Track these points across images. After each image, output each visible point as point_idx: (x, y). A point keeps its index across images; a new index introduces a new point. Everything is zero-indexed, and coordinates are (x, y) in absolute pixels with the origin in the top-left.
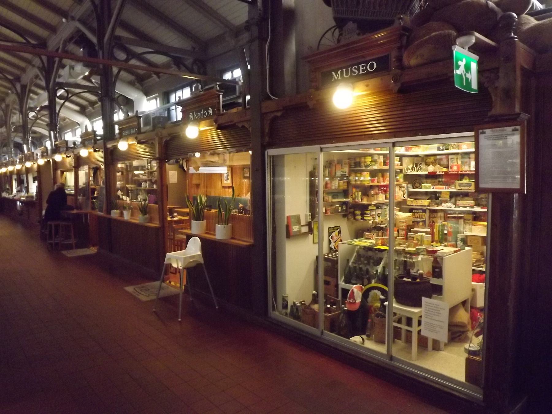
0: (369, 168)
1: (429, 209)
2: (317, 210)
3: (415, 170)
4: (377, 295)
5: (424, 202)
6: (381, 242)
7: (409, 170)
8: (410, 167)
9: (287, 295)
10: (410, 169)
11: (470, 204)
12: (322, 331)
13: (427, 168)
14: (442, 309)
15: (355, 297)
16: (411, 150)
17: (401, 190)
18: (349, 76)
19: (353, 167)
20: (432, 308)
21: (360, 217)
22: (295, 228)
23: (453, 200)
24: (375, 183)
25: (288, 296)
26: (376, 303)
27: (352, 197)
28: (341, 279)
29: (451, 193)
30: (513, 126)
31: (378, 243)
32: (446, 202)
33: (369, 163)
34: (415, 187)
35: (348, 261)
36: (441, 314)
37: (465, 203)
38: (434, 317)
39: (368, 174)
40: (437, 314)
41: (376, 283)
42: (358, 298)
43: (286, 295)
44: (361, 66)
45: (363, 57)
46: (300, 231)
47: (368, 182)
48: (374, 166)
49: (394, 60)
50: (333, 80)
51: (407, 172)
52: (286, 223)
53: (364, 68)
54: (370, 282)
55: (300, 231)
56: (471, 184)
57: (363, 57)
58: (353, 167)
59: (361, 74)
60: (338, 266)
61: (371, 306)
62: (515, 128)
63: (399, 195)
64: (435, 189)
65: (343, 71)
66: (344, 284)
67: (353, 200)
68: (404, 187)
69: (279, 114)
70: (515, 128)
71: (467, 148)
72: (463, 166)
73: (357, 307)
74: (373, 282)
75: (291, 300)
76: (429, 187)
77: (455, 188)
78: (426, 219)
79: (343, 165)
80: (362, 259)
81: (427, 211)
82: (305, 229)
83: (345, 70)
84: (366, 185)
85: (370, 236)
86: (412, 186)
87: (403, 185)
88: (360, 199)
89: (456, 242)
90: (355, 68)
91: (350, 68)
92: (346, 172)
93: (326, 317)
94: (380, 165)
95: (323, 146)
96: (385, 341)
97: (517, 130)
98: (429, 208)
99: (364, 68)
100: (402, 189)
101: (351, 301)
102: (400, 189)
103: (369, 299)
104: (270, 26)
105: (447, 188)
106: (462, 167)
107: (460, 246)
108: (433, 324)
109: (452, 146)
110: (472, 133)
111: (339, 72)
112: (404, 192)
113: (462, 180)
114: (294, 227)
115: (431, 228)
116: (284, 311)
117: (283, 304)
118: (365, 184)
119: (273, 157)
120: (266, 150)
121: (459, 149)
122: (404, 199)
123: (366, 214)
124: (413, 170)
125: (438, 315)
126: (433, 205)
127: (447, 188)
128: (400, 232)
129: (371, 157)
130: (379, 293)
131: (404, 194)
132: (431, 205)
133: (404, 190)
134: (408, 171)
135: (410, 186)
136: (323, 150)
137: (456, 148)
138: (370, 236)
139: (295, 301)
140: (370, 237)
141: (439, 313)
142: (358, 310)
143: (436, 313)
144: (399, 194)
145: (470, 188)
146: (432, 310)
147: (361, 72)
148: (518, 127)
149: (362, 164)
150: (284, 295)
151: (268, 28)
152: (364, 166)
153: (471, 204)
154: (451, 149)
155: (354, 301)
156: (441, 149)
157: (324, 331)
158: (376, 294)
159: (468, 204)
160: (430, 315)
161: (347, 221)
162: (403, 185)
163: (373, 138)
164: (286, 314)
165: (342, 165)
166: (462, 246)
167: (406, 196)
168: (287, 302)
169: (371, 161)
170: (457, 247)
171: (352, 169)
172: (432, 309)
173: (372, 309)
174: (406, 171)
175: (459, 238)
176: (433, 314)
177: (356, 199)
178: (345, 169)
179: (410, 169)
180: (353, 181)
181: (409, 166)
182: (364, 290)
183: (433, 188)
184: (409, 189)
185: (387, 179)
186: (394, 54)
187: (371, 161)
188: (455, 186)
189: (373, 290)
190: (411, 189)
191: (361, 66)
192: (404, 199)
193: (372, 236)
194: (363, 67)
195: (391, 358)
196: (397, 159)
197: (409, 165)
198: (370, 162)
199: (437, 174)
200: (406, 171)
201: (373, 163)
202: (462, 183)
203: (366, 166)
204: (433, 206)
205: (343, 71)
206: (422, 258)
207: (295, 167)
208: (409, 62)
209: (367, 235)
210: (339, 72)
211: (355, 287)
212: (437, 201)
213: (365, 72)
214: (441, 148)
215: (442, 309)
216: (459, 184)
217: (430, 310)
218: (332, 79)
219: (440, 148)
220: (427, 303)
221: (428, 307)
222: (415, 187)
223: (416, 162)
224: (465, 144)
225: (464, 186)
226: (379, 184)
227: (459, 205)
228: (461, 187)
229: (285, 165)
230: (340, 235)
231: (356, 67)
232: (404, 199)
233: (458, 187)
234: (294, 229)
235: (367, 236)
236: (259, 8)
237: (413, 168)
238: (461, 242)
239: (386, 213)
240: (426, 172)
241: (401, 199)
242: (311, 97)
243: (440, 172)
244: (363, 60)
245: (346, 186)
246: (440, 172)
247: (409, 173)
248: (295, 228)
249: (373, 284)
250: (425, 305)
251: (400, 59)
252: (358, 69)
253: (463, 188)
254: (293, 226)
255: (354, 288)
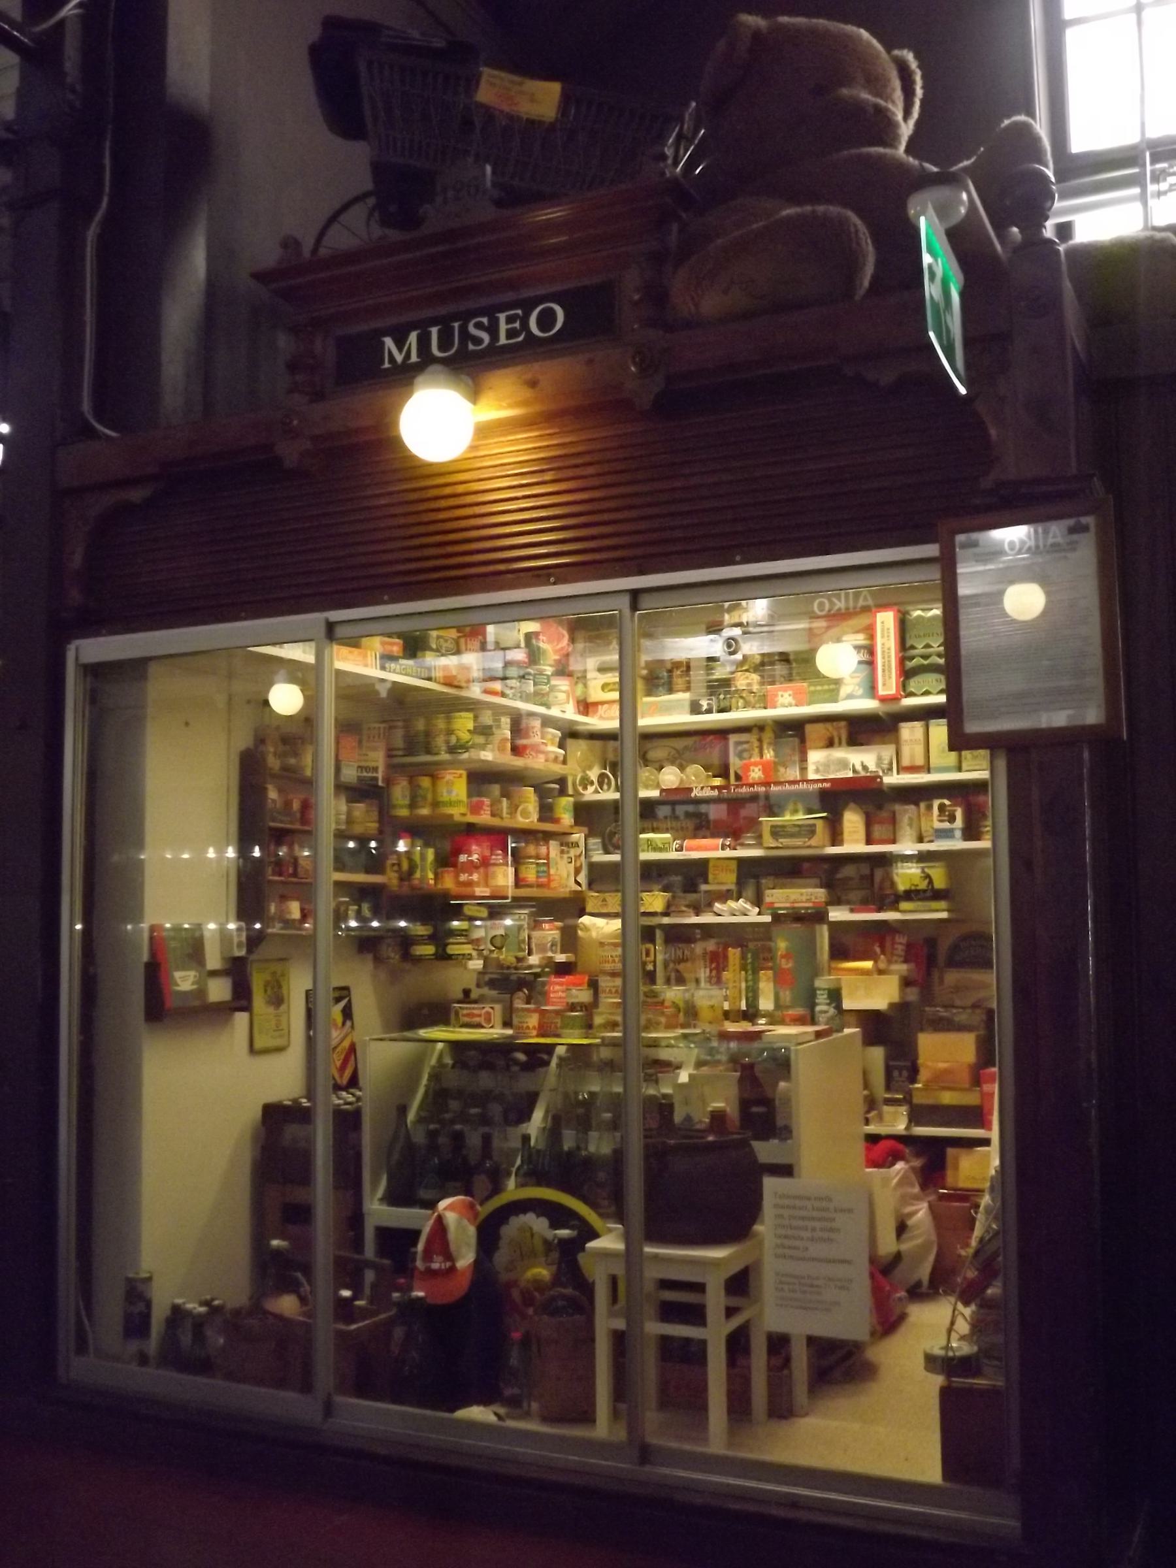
0: (465, 756)
1: (662, 927)
2: (269, 910)
3: (609, 784)
4: (532, 1235)
5: (650, 900)
6: (536, 1024)
7: (589, 787)
8: (593, 775)
9: (148, 1275)
10: (592, 783)
11: (813, 898)
12: (329, 1394)
13: (658, 778)
14: (842, 1211)
15: (453, 1247)
16: (596, 712)
17: (565, 856)
18: (446, 354)
19: (400, 753)
20: (803, 1213)
21: (429, 950)
22: (184, 981)
23: (750, 891)
24: (484, 818)
25: (150, 1279)
26: (528, 1268)
27: (396, 871)
28: (375, 1186)
29: (741, 861)
30: (1070, 516)
31: (528, 1028)
32: (724, 896)
33: (465, 736)
34: (611, 849)
35: (403, 1110)
36: (838, 1230)
37: (793, 897)
38: (815, 1250)
39: (460, 776)
40: (826, 1235)
41: (520, 1185)
42: (464, 1250)
43: (145, 1275)
44: (502, 317)
45: (511, 285)
46: (201, 992)
47: (463, 810)
48: (484, 750)
49: (636, 297)
50: (387, 365)
51: (582, 791)
52: (145, 957)
53: (517, 325)
54: (497, 1189)
55: (201, 992)
56: (814, 825)
57: (511, 285)
58: (400, 753)
59: (504, 346)
60: (359, 1139)
61: (513, 1284)
62: (1078, 523)
63: (559, 875)
64: (687, 850)
65: (429, 334)
66: (385, 1208)
67: (401, 879)
68: (577, 845)
69: (137, 495)
70: (1078, 523)
71: (793, 702)
72: (782, 770)
73: (459, 1287)
74: (511, 1183)
75: (163, 1298)
76: (664, 844)
77: (759, 844)
78: (655, 966)
79: (364, 743)
80: (454, 1105)
81: (659, 935)
82: (219, 990)
83: (439, 332)
84: (458, 818)
85: (480, 1016)
86: (600, 846)
87: (575, 837)
88: (431, 875)
89: (812, 1005)
90: (479, 326)
91: (456, 325)
92: (375, 769)
93: (340, 1335)
94: (501, 749)
95: (335, 615)
96: (592, 1404)
97: (1084, 529)
98: (666, 920)
99: (517, 325)
100: (568, 852)
101: (435, 1266)
102: (562, 852)
103: (501, 1257)
104: (107, 161)
105: (729, 846)
106: (778, 771)
107: (825, 1020)
108: (809, 1277)
109: (744, 695)
110: (931, 550)
111: (413, 337)
112: (578, 865)
113: (783, 816)
114: (178, 975)
115: (714, 965)
116: (133, 1346)
117: (128, 1318)
118: (451, 816)
119: (95, 672)
120: (69, 643)
121: (765, 708)
122: (579, 888)
123: (453, 933)
124: (605, 787)
125: (830, 1240)
126: (684, 909)
127: (729, 846)
128: (605, 983)
129: (470, 715)
130: (538, 1224)
131: (577, 871)
132: (673, 908)
133: (575, 856)
134: (585, 788)
135: (595, 842)
136: (340, 631)
137: (758, 705)
138: (480, 1016)
139: (179, 1301)
140: (477, 1020)
141: (831, 1230)
142: (466, 1297)
143: (822, 1230)
144: (559, 872)
145: (813, 842)
146: (806, 1223)
147: (503, 340)
148: (1089, 520)
149: (440, 741)
150: (131, 1275)
151: (102, 167)
152: (444, 748)
153: (816, 898)
154: (737, 708)
155: (448, 1264)
156: (705, 707)
157: (339, 1399)
158: (531, 1229)
159: (804, 898)
160: (797, 1243)
161: (376, 968)
162: (575, 837)
163: (552, 579)
164: (143, 1360)
165: (360, 742)
166: (832, 1018)
167: (582, 878)
168: (149, 1304)
169: (471, 728)
170: (813, 1022)
171: (396, 760)
172: (803, 1218)
173: (516, 1294)
174: (580, 789)
175: (820, 989)
176: (812, 1239)
177: (418, 875)
178: (372, 755)
179: (592, 783)
180: (402, 807)
181: (588, 772)
182: (482, 1217)
183: (680, 849)
184: (592, 857)
185: (520, 809)
186: (631, 284)
187: (471, 728)
188: (759, 837)
189: (517, 1215)
190: (599, 857)
191: (502, 317)
192: (576, 892)
193: (488, 1014)
194: (510, 320)
195: (645, 1454)
196: (554, 736)
197: (590, 768)
198: (469, 731)
199: (693, 795)
200: (580, 789)
201: (480, 740)
202: (783, 827)
203: (452, 750)
204: (683, 911)
205: (430, 332)
206: (690, 1076)
207: (187, 724)
208: (696, 305)
209: (465, 1012)
210: (413, 337)
211: (450, 1208)
212: (692, 897)
213: (521, 339)
214: (704, 704)
215: (842, 1211)
216: (772, 827)
217: (795, 1223)
218: (383, 362)
219: (701, 706)
220: (783, 1196)
221: (786, 1213)
222: (611, 849)
223: (611, 756)
224: (785, 690)
225: (792, 835)
226: (496, 822)
227: (773, 903)
228: (781, 840)
229: (150, 711)
230: (348, 1023)
231: (485, 320)
232: (579, 888)
233: (769, 841)
234: (179, 981)
235: (468, 1015)
236: (69, 80)
237: (602, 778)
238: (829, 1004)
239: (521, 938)
240: (653, 789)
241: (568, 890)
242: (295, 422)
243: (702, 788)
244: (510, 296)
245: (376, 825)
246: (702, 788)
247: (590, 794)
248: (184, 979)
249: (513, 1190)
250: (776, 1206)
251: (657, 296)
252: (493, 330)
253: (785, 841)
254: (177, 969)
255: (445, 1209)
